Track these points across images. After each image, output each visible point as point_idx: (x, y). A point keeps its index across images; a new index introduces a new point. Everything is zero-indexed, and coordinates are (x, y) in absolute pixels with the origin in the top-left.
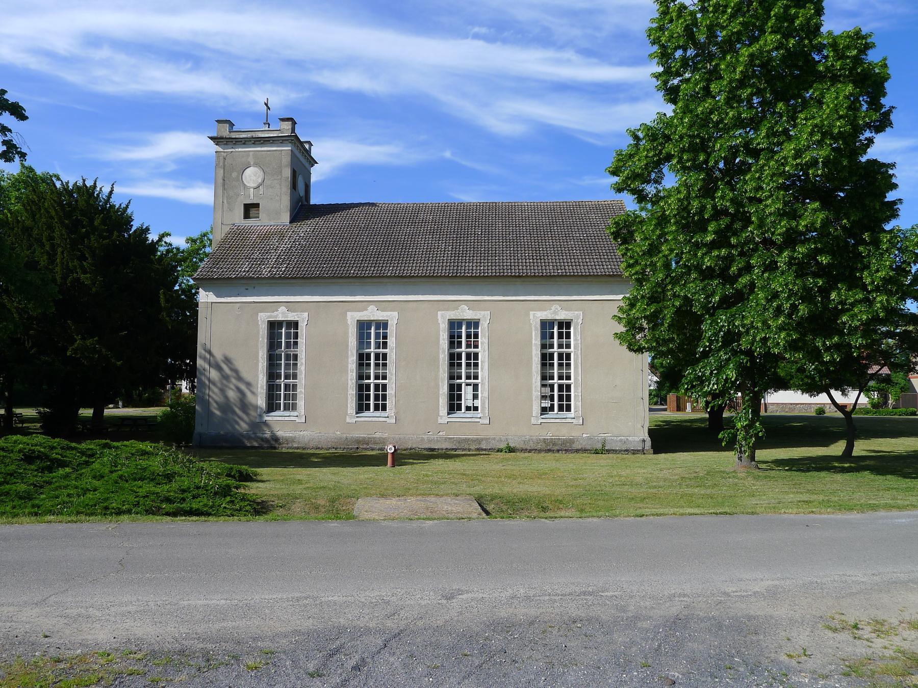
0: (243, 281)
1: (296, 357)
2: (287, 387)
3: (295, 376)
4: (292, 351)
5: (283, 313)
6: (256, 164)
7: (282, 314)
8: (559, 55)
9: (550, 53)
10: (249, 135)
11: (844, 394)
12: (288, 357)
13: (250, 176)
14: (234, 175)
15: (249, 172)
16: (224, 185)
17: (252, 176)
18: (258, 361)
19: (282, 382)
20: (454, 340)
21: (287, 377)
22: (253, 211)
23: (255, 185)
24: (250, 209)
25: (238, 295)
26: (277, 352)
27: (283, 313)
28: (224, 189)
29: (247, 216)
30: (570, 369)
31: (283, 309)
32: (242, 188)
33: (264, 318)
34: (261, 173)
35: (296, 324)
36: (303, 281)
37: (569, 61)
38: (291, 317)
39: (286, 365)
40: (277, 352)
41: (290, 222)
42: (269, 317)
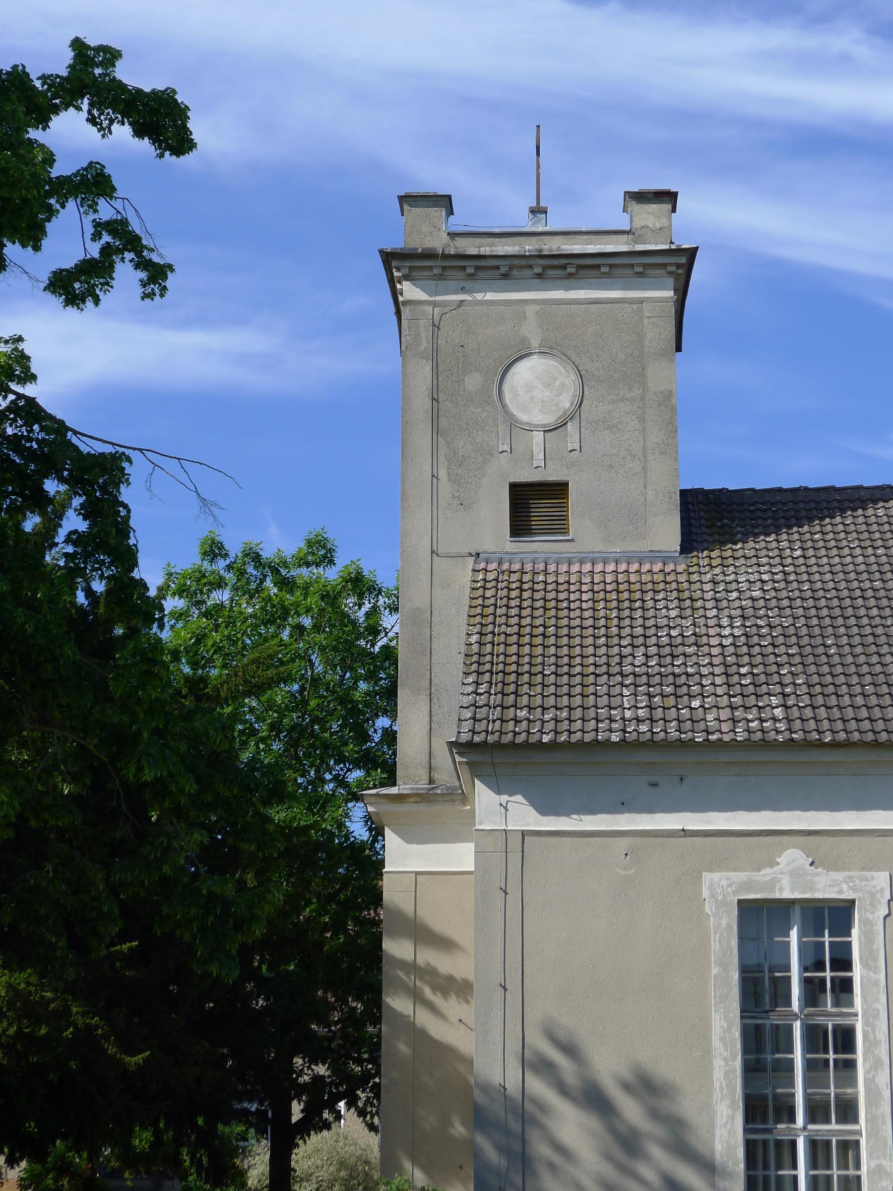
0: (644, 756)
1: (845, 1039)
2: (819, 1150)
3: (848, 1111)
4: (829, 1015)
5: (796, 874)
6: (546, 351)
7: (789, 877)
8: (810, 41)
9: (782, 37)
10: (529, 246)
11: (185, 1161)
12: (815, 1038)
13: (530, 388)
14: (473, 382)
15: (525, 372)
16: (435, 417)
17: (536, 387)
18: (707, 1051)
19: (800, 1130)
20: (759, 990)
21: (817, 1111)
22: (540, 510)
23: (549, 419)
24: (534, 504)
25: (622, 806)
26: (775, 1019)
27: (796, 874)
28: (436, 430)
29: (520, 527)
30: (853, 1083)
31: (792, 857)
32: (502, 428)
33: (722, 889)
34: (568, 379)
35: (839, 915)
36: (873, 755)
37: (844, 64)
38: (827, 886)
39: (810, 1066)
40: (775, 1019)
41: (687, 547)
42: (748, 886)
